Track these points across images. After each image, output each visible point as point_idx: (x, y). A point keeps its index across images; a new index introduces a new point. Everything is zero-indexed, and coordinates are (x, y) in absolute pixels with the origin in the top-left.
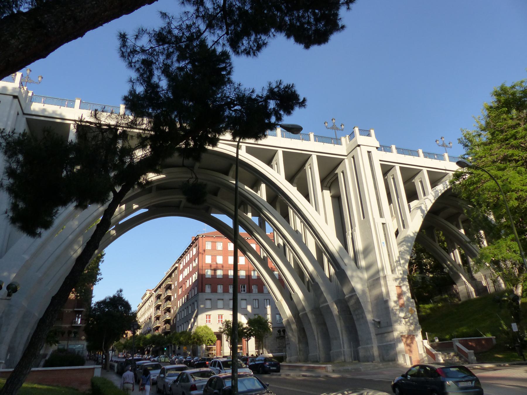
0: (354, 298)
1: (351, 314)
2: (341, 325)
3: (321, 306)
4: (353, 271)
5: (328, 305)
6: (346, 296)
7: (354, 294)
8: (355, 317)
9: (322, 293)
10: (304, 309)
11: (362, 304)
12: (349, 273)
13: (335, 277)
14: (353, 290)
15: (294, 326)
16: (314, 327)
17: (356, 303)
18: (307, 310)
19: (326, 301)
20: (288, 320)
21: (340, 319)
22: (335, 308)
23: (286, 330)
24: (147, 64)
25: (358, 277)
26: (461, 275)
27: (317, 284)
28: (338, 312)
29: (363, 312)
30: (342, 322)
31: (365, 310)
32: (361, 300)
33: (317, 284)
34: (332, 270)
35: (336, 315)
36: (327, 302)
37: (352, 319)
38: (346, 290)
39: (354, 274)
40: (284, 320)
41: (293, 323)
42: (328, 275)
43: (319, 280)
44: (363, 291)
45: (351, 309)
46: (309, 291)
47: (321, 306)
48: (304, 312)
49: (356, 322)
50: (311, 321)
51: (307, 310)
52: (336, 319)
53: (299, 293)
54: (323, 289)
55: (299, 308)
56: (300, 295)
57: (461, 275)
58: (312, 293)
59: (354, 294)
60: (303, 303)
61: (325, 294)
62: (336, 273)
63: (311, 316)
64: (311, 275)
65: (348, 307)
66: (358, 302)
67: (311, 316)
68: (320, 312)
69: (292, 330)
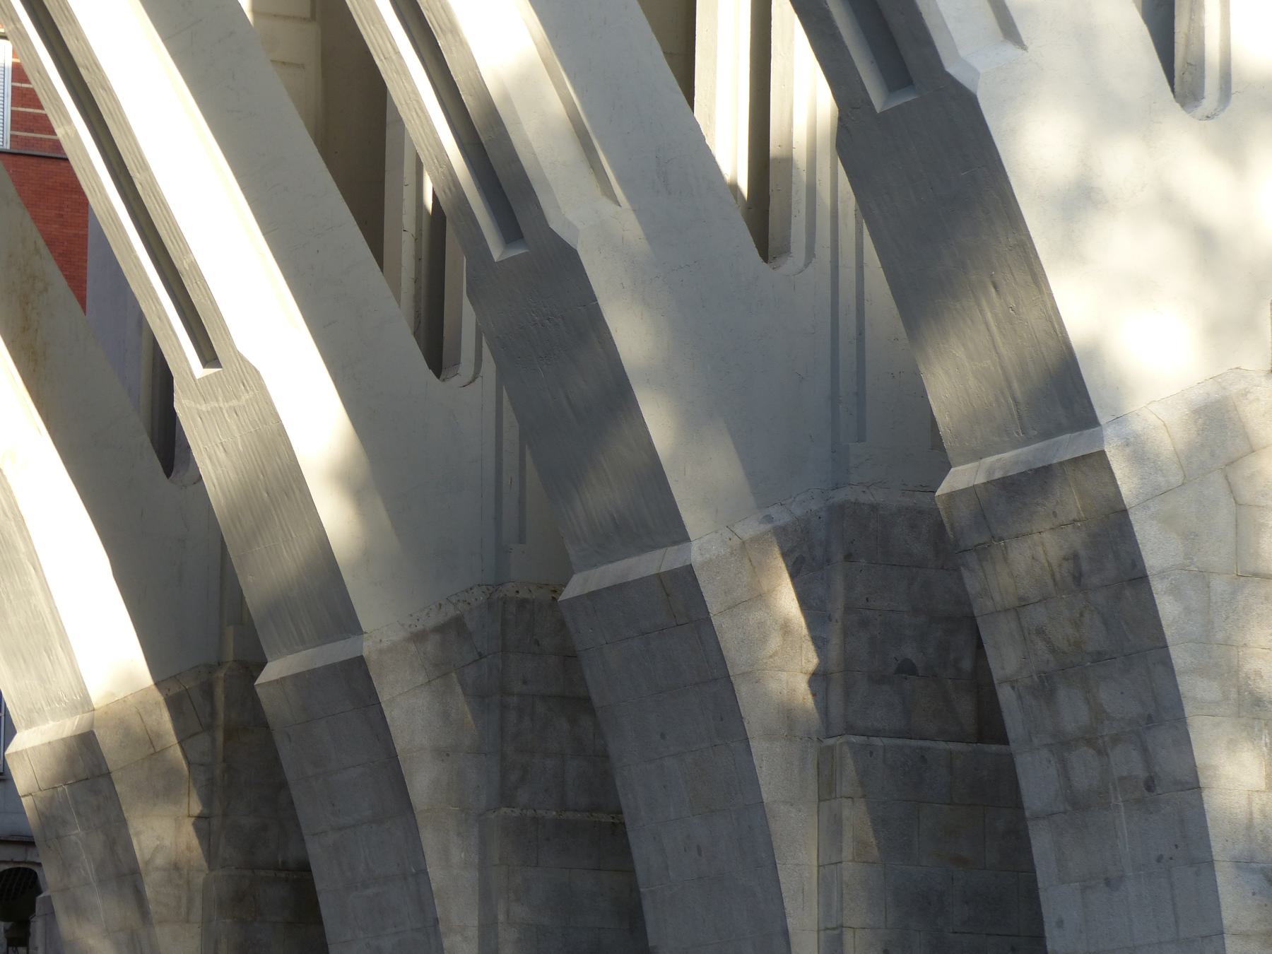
0: (1071, 500)
1: (989, 727)
2: (828, 867)
3: (575, 588)
4: (1110, 114)
5: (687, 576)
6: (962, 477)
7: (1068, 447)
8: (1037, 781)
9: (617, 395)
10: (324, 596)
11: (1168, 608)
12: (1040, 144)
13: (833, 186)
14: (1063, 392)
15: (163, 833)
16: (451, 864)
17: (1076, 576)
18: (382, 624)
19: (658, 519)
20: (85, 743)
21: (827, 789)
22: (778, 641)
23: (50, 876)
24: (220, 664)
25: (1168, 205)
26: (249, 16)
27: (563, 261)
28: (818, 679)
29: (1163, 716)
30: (855, 816)
31: (1195, 689)
32: (1157, 547)
33: (560, 265)
34: (807, 100)
35: (788, 715)
36: (673, 530)
37: (996, 794)
38: (957, 378)
39: (1122, 163)
40: (35, 743)
41: (163, 788)
42: (733, 162)
43: (591, 215)
44: (1218, 424)
45: (1006, 660)
46: (437, 355)
47: (575, 588)
48: (337, 652)
49: (1041, 843)
50: (423, 782)
51: (383, 624)
52: (776, 771)
53: (279, 385)
54: (633, 333)
55: (267, 572)
56: (317, 425)
57: (249, 16)
58: (472, 398)
59: (1068, 447)
60: (335, 514)
61: (659, 420)
62: (854, 132)
63: (414, 713)
64: (483, 134)
65: (965, 626)
66: (1110, 560)
67: (414, 713)
68: (559, 653)
69: (125, 875)
